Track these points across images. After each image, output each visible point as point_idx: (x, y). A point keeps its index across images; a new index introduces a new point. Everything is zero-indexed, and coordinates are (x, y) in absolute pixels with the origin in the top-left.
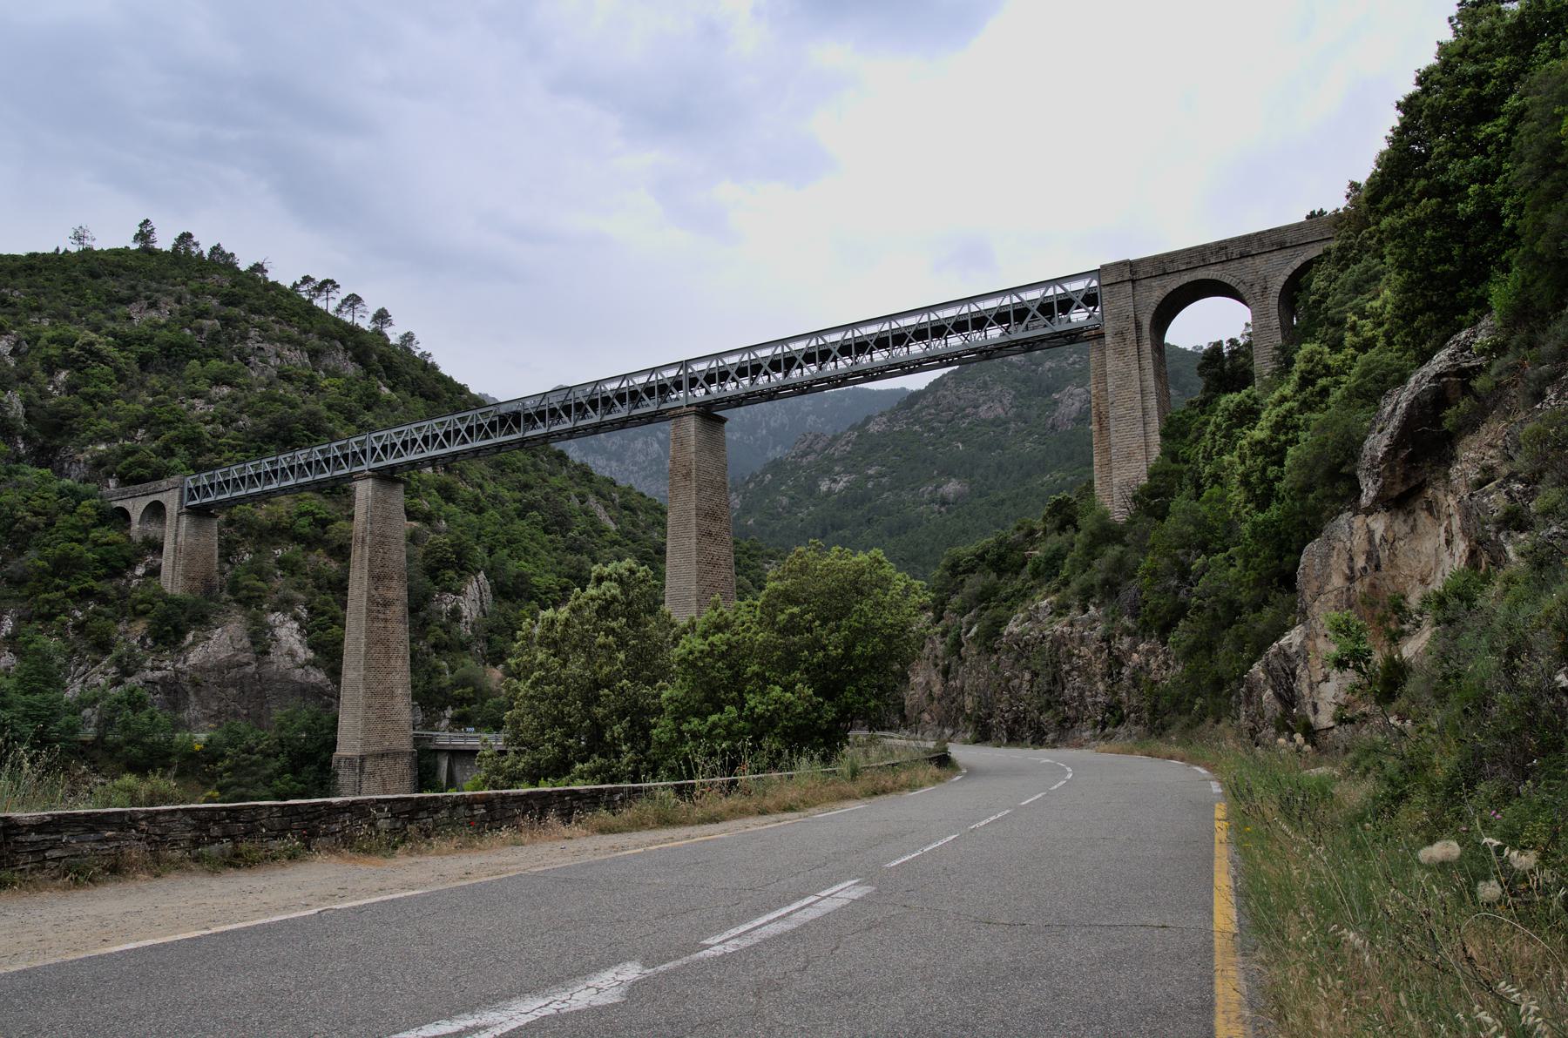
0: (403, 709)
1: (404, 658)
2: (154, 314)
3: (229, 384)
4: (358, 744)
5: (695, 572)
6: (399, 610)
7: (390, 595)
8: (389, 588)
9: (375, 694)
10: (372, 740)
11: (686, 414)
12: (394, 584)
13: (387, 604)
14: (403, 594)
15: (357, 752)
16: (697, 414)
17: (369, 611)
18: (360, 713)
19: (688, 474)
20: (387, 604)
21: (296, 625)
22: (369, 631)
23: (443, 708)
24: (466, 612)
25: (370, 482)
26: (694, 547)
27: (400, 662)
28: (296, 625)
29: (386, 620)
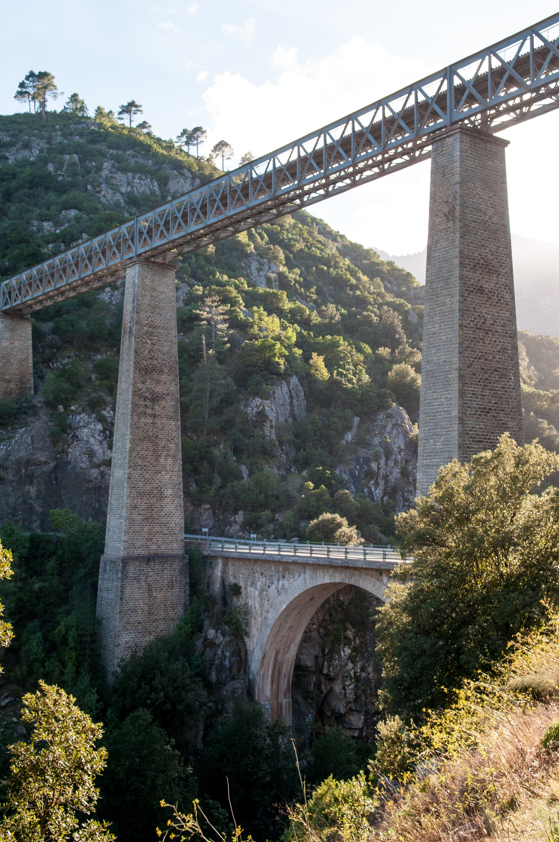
0: (173, 510)
1: (174, 456)
2: (26, 153)
3: (76, 208)
4: (121, 546)
5: (457, 341)
6: (169, 405)
7: (159, 389)
8: (158, 382)
9: (141, 494)
10: (138, 544)
12: (164, 377)
13: (155, 398)
14: (174, 388)
15: (122, 553)
17: (135, 405)
18: (124, 514)
20: (155, 398)
21: (99, 427)
23: (235, 512)
24: (272, 415)
25: (137, 267)
26: (456, 306)
27: (170, 461)
28: (99, 427)
29: (154, 416)
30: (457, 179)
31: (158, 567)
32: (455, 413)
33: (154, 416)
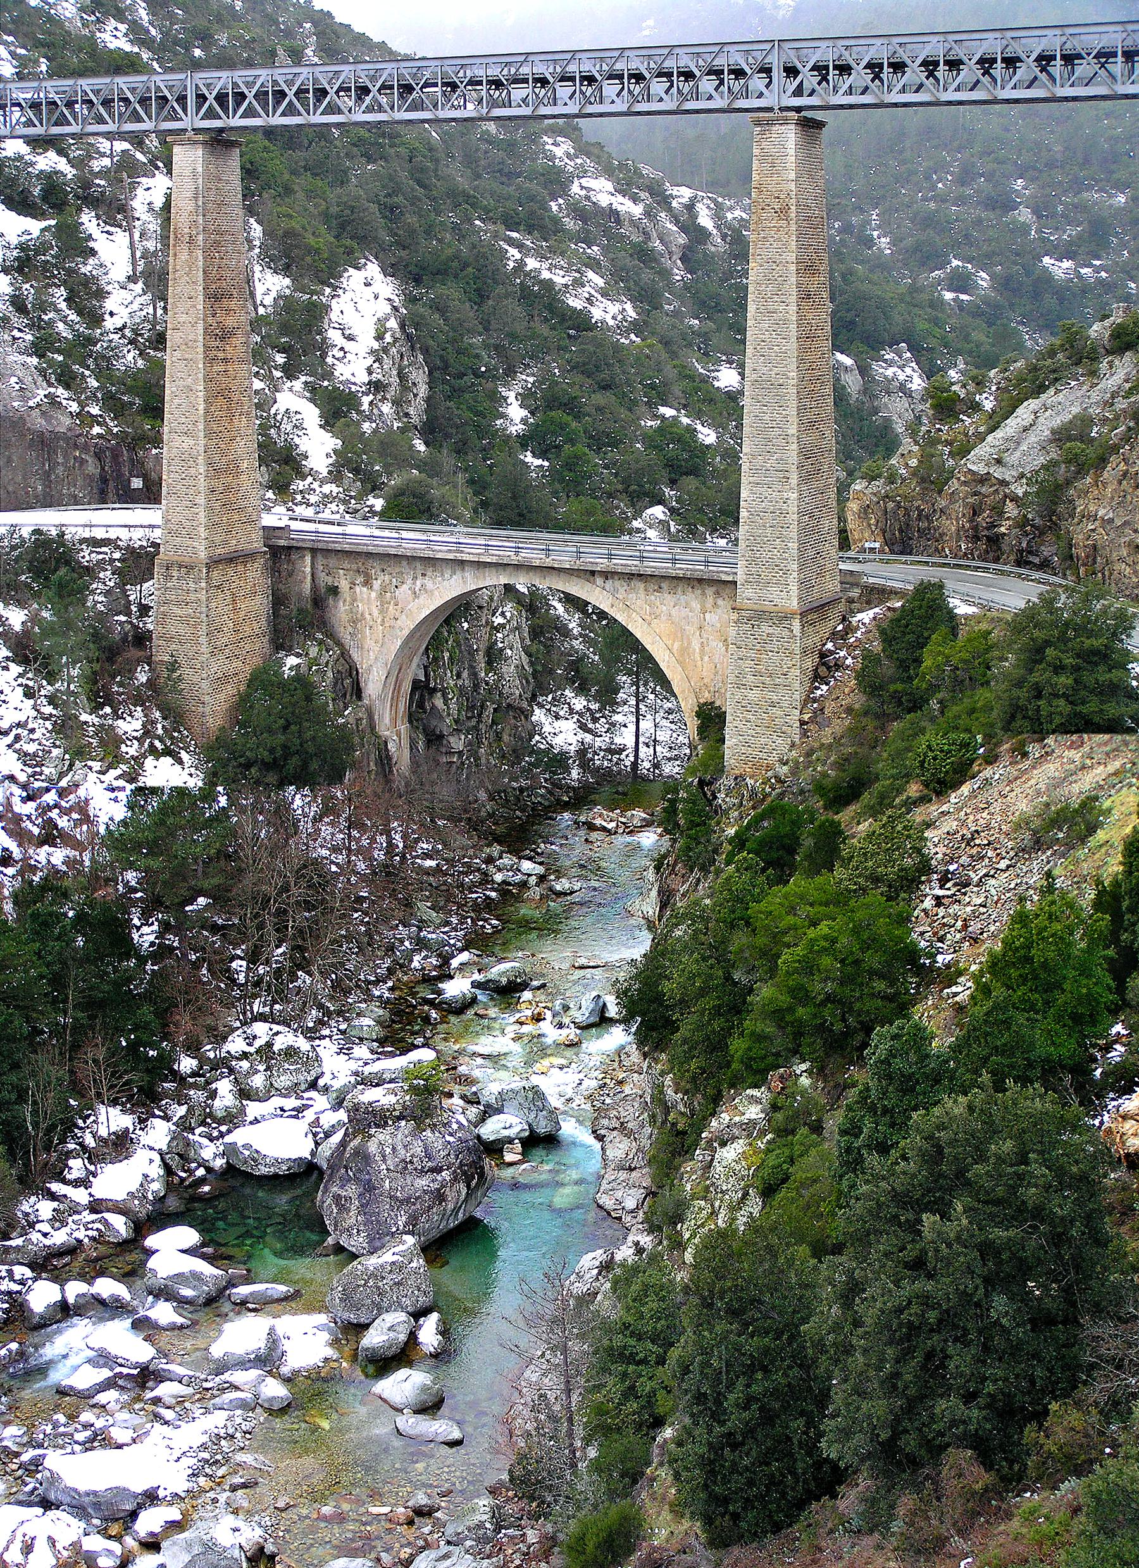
7: (230, 322)
11: (785, 122)
19: (783, 212)
22: (208, 379)
30: (792, 176)
31: (240, 568)
32: (793, 430)
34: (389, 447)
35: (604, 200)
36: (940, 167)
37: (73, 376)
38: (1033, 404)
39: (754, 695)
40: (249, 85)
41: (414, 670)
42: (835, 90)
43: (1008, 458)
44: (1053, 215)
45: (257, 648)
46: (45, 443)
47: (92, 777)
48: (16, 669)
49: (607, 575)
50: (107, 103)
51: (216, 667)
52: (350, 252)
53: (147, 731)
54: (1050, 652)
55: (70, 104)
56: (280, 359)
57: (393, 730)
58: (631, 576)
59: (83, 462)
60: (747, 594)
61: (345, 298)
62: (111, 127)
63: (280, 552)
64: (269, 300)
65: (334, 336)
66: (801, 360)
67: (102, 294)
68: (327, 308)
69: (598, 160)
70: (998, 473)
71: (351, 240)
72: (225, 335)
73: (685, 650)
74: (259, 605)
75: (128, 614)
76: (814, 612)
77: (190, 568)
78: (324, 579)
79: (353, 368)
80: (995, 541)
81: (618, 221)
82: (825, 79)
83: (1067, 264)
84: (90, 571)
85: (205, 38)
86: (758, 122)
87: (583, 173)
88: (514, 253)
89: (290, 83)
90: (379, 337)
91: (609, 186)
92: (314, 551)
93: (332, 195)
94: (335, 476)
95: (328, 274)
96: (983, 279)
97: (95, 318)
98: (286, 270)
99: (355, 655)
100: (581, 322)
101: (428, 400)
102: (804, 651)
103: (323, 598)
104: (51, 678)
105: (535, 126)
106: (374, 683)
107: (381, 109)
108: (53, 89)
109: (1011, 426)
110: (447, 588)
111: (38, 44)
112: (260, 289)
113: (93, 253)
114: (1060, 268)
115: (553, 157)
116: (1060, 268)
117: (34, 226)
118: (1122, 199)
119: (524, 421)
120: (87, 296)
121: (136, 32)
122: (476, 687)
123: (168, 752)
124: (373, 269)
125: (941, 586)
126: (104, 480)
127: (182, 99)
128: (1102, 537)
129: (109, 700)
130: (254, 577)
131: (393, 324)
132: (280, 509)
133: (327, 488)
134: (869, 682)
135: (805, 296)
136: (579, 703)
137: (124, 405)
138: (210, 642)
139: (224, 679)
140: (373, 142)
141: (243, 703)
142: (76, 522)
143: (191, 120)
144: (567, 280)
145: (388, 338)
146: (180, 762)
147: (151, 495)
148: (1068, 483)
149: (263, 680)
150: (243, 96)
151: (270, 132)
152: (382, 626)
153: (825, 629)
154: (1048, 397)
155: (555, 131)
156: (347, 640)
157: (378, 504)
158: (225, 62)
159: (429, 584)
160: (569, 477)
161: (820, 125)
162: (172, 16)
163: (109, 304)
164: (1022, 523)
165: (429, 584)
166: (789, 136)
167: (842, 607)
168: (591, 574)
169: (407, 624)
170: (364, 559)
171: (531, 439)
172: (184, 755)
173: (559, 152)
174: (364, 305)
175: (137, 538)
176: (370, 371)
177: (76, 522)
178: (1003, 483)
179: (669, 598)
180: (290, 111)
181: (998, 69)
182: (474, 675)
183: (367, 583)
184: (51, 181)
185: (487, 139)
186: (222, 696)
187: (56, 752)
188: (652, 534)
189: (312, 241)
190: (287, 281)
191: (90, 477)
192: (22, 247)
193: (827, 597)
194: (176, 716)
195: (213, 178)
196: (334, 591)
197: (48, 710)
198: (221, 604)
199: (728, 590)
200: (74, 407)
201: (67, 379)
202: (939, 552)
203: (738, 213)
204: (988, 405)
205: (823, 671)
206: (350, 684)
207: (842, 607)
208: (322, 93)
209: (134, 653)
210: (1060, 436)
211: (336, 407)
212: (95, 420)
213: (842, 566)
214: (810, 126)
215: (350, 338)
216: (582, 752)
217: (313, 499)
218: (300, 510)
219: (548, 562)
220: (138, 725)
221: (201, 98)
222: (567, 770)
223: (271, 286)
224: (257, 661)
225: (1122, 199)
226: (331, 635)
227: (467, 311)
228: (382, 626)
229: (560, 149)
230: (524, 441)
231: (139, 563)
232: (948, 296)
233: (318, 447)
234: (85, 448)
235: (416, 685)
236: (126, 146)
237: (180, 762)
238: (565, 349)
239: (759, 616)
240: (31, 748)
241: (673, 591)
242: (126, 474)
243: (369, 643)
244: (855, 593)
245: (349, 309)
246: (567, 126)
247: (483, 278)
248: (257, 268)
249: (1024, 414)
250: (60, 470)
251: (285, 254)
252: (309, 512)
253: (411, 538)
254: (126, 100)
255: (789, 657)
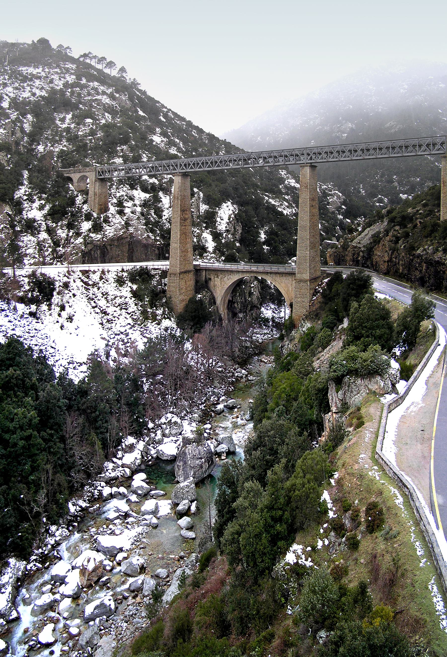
7: (186, 216)
8: (186, 214)
11: (307, 166)
16: (310, 166)
19: (307, 186)
22: (180, 230)
29: (185, 226)
32: (308, 237)
33: (185, 226)
34: (229, 245)
35: (293, 185)
36: (377, 174)
37: (154, 230)
38: (368, 229)
39: (299, 299)
40: (200, 161)
41: (229, 297)
42: (342, 156)
43: (362, 242)
44: (403, 184)
45: (191, 293)
46: (146, 246)
47: (149, 324)
48: (133, 299)
49: (271, 273)
50: (168, 166)
51: (181, 297)
52: (223, 199)
53: (164, 313)
54: (351, 285)
55: (168, 166)
56: (204, 225)
57: (223, 311)
58: (276, 273)
59: (154, 250)
60: (298, 276)
61: (222, 210)
62: (169, 172)
63: (198, 270)
64: (203, 211)
65: (218, 219)
66: (310, 221)
67: (163, 211)
68: (217, 213)
69: (292, 175)
70: (359, 245)
71: (225, 197)
72: (185, 220)
73: (288, 290)
74: (192, 283)
75: (162, 286)
76: (313, 280)
77: (175, 274)
78: (208, 276)
79: (222, 226)
80: (358, 261)
81: (296, 190)
82: (363, 152)
83: (406, 195)
84: (153, 276)
85: (196, 150)
86: (301, 167)
87: (288, 178)
88: (267, 198)
89: (237, 158)
90: (229, 219)
91: (294, 181)
92: (206, 270)
93: (222, 185)
94: (214, 252)
95: (219, 205)
96: (386, 200)
97: (160, 217)
98: (208, 204)
99: (215, 294)
100: (281, 213)
101: (241, 233)
102: (310, 289)
103: (207, 281)
104: (141, 301)
105: (277, 167)
106: (219, 300)
107: (183, 169)
108: (157, 163)
109: (363, 234)
110: (235, 278)
111: (154, 153)
112: (201, 208)
113: (161, 201)
114: (404, 196)
115: (281, 175)
116: (404, 196)
117: (148, 196)
118: (418, 179)
119: (265, 238)
120: (159, 212)
121: (179, 150)
122: (246, 301)
123: (168, 318)
124: (229, 203)
125: (342, 272)
126: (160, 255)
127: (177, 166)
128: (378, 259)
129: (156, 306)
130: (191, 276)
131: (233, 216)
132: (201, 260)
133: (212, 255)
134: (324, 295)
135: (312, 206)
136: (273, 306)
137: (165, 237)
138: (180, 292)
139: (183, 300)
140: (234, 173)
141: (187, 306)
142: (150, 265)
143: (178, 170)
144: (279, 204)
145: (231, 219)
146: (171, 320)
147: (167, 259)
148: (373, 247)
149: (192, 301)
150: (198, 164)
151: (208, 172)
152: (221, 287)
153: (316, 284)
154: (372, 227)
155: (282, 169)
156: (212, 290)
157: (223, 258)
158: (200, 155)
159: (231, 277)
160: (274, 251)
161: (316, 167)
162: (188, 145)
163: (164, 213)
164: (363, 257)
165: (231, 277)
166: (307, 170)
167: (321, 278)
168: (267, 273)
169: (226, 286)
170: (217, 271)
171: (267, 242)
172: (172, 319)
173: (283, 173)
174: (226, 211)
175: (164, 268)
176: (226, 227)
177: (150, 265)
178: (360, 248)
179: (285, 278)
180: (200, 167)
181: (431, 147)
182: (245, 298)
183: (217, 277)
184: (153, 184)
185: (266, 171)
186: (182, 305)
187: (141, 318)
188: (293, 264)
189: (214, 197)
190: (208, 207)
191: (156, 254)
192: (145, 201)
193: (317, 276)
194: (171, 310)
195: (183, 183)
196: (210, 279)
197: (140, 308)
198: (183, 283)
199: (294, 276)
200: (153, 238)
201: (152, 231)
202: (346, 265)
203: (325, 187)
204: (360, 230)
205: (315, 293)
206: (213, 301)
207: (321, 278)
208: (189, 164)
209: (162, 295)
210: (373, 236)
211: (216, 236)
212: (158, 240)
213: (321, 269)
214: (313, 167)
215: (222, 220)
216: (273, 317)
217: (208, 258)
218: (205, 260)
219: (257, 271)
220: (161, 312)
221: (181, 165)
222: (269, 322)
223: (204, 208)
224: (191, 296)
225: (418, 179)
226: (208, 289)
227: (253, 213)
228: (221, 287)
229: (283, 173)
230: (264, 243)
231: (164, 274)
232: (378, 204)
233: (211, 245)
234: (155, 247)
235: (229, 301)
236: (171, 176)
237: (171, 320)
238: (276, 220)
239: (301, 281)
240: (135, 317)
241: (285, 276)
242: (162, 253)
243: (218, 291)
244: (325, 275)
245: (223, 213)
246: (285, 167)
247: (258, 204)
248: (201, 204)
249: (366, 231)
250: (149, 253)
251: (208, 200)
252: (206, 261)
253: (228, 266)
254: (173, 166)
255: (306, 289)
